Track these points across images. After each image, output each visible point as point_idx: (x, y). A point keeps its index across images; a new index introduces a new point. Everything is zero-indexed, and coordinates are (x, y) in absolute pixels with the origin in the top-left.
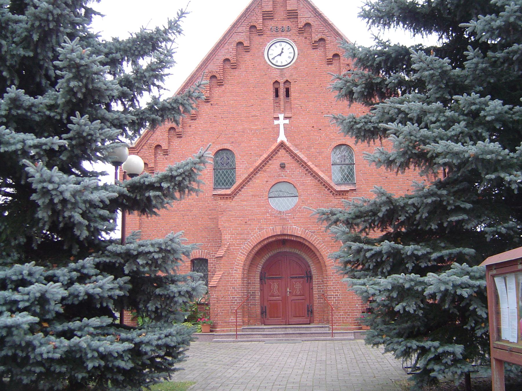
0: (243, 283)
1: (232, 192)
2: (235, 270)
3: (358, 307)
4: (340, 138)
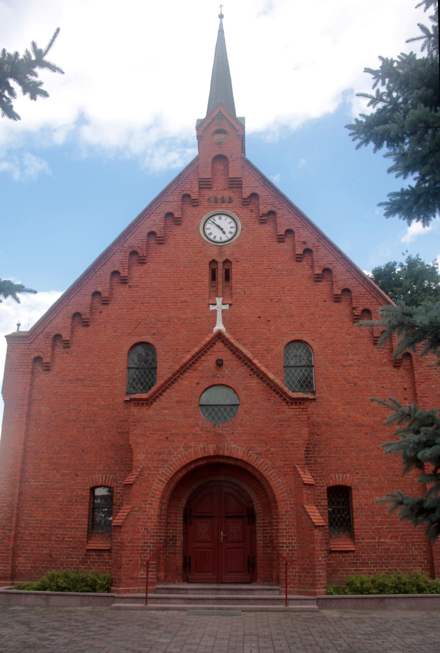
0: (160, 522)
1: (151, 397)
2: (149, 504)
3: (321, 561)
4: (294, 332)
